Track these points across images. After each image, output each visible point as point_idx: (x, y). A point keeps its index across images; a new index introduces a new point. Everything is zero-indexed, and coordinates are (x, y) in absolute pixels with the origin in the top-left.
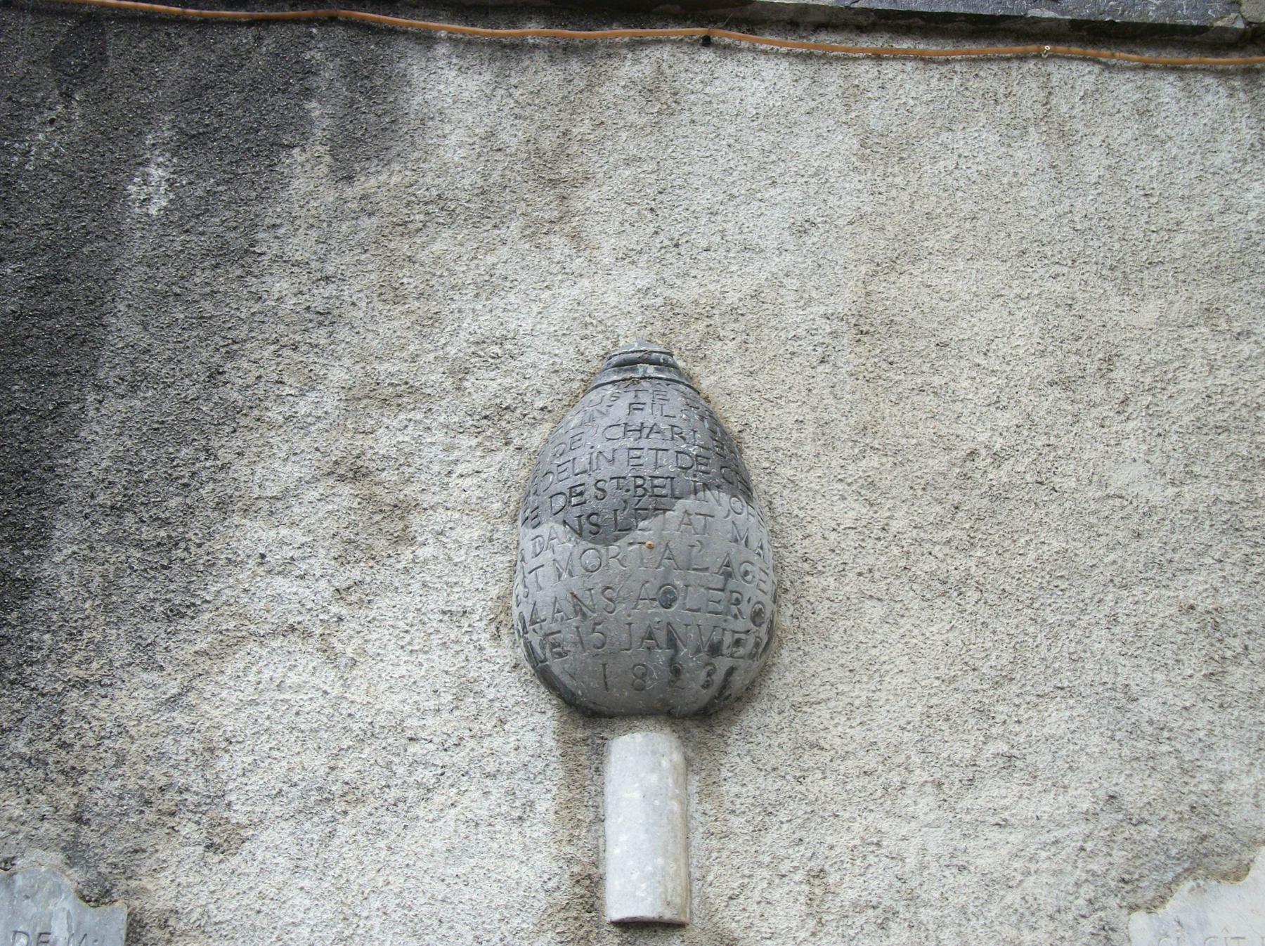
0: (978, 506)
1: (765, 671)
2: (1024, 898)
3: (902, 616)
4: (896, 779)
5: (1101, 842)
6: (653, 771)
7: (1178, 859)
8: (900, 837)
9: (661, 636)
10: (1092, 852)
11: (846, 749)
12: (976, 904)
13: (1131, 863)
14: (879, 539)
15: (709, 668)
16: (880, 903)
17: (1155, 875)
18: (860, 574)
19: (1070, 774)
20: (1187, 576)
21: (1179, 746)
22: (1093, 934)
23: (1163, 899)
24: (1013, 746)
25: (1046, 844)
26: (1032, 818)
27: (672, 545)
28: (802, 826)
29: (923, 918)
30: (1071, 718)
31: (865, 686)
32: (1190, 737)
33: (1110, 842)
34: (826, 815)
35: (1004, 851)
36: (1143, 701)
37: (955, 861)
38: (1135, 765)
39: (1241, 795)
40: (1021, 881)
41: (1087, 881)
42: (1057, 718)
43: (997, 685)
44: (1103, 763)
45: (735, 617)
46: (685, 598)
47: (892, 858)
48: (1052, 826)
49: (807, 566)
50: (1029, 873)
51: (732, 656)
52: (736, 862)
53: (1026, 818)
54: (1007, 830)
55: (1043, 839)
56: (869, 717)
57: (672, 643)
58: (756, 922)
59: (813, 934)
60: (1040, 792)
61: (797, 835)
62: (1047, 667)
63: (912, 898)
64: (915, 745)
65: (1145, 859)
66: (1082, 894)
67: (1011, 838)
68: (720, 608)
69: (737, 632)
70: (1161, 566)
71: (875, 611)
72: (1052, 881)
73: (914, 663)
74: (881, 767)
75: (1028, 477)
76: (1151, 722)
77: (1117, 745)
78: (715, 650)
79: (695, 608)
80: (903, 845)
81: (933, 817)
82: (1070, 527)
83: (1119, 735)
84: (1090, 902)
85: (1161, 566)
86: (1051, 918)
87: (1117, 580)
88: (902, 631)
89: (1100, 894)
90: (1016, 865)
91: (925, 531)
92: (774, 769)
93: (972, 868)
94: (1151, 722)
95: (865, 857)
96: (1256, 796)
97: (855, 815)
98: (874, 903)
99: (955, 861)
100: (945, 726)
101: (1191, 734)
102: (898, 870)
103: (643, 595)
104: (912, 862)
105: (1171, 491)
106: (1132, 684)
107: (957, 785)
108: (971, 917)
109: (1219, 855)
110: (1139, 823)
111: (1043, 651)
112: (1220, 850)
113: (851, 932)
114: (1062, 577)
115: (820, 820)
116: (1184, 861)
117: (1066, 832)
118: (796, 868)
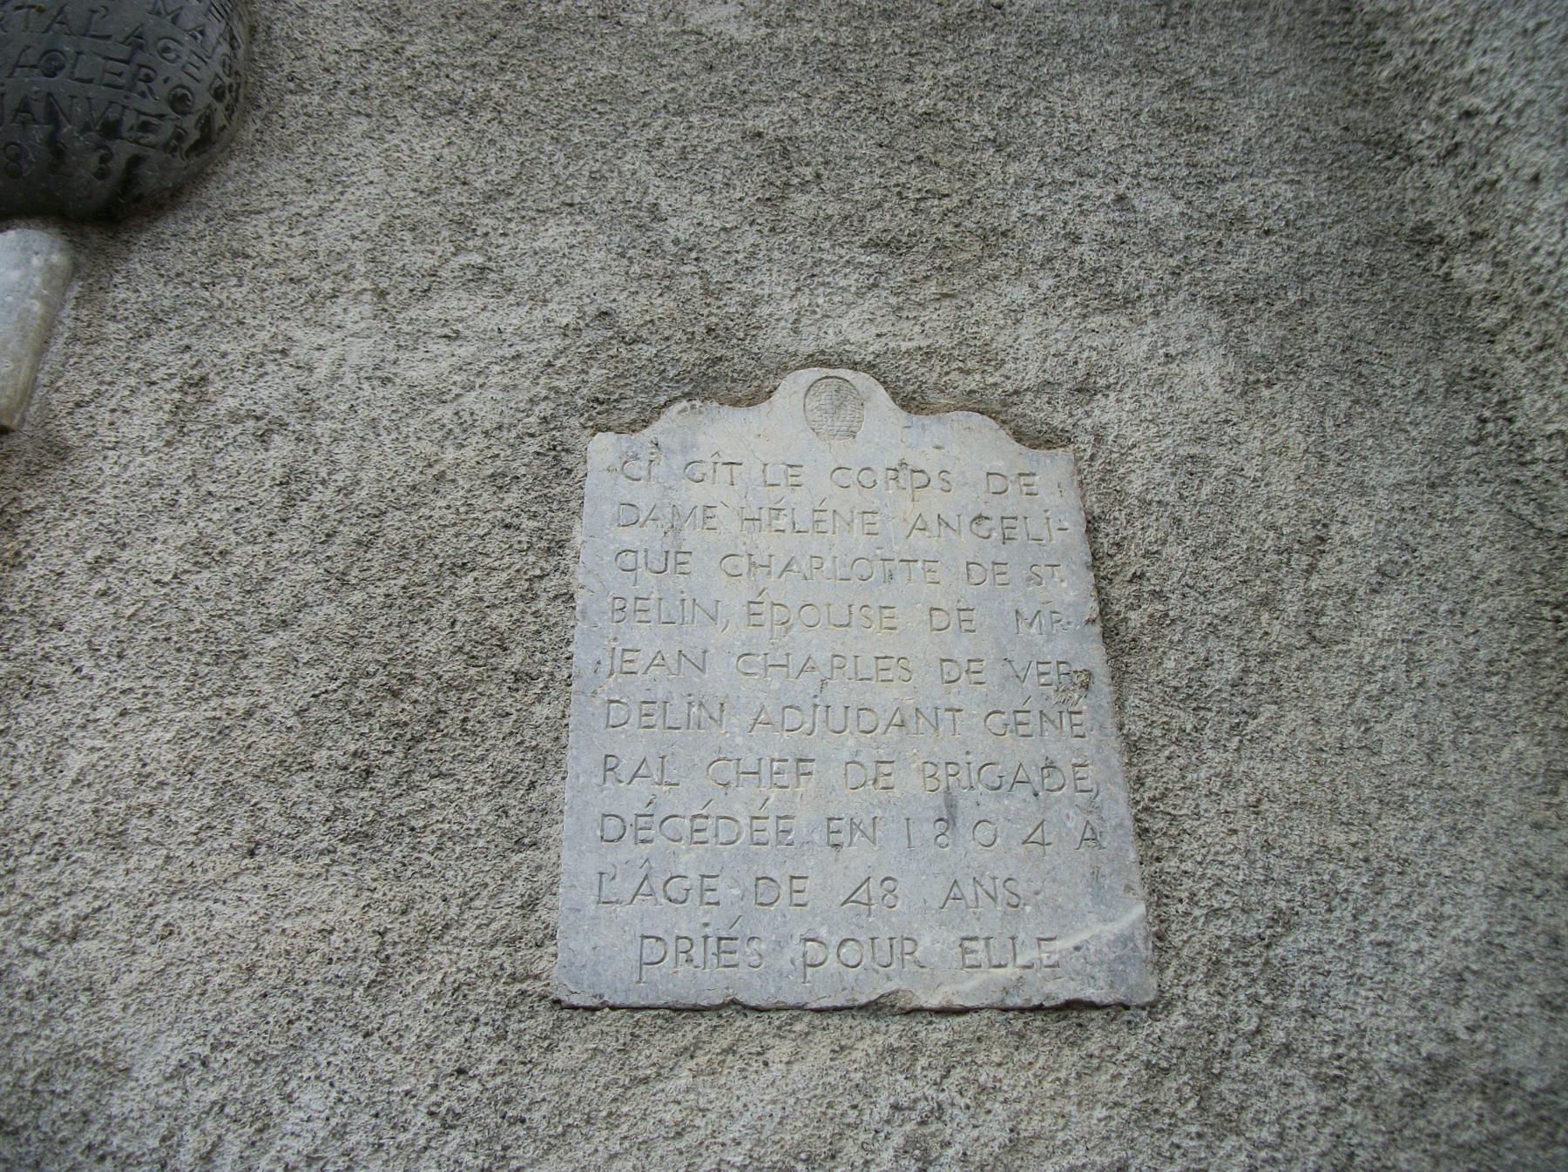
0: (520, 34)
1: (199, 178)
2: (457, 414)
3: (392, 132)
4: (327, 287)
5: (577, 360)
6: (17, 267)
7: (678, 382)
8: (315, 345)
9: (39, 109)
10: (562, 368)
11: (276, 256)
12: (393, 417)
13: (612, 382)
14: (387, 61)
15: (102, 152)
16: (267, 414)
17: (642, 398)
18: (353, 92)
19: (556, 287)
20: (762, 107)
21: (707, 268)
22: (538, 453)
23: (646, 423)
24: (490, 259)
25: (503, 358)
26: (492, 330)
27: (67, 9)
28: (195, 333)
29: (318, 431)
30: (574, 233)
31: (322, 197)
32: (724, 259)
33: (591, 357)
34: (228, 323)
35: (444, 365)
36: (673, 221)
37: (378, 373)
38: (644, 282)
39: (778, 320)
40: (458, 396)
41: (546, 398)
42: (554, 234)
43: (489, 198)
44: (603, 278)
45: (143, 95)
46: (74, 66)
47: (298, 368)
48: (516, 339)
49: (291, 85)
50: (473, 388)
51: (136, 142)
52: (99, 367)
53: (485, 330)
54: (459, 343)
55: (500, 353)
56: (316, 226)
57: (53, 116)
58: (101, 431)
59: (169, 444)
60: (511, 305)
61: (186, 341)
62: (557, 183)
63: (310, 409)
64: (365, 254)
65: (632, 379)
66: (537, 413)
67: (461, 352)
68: (122, 81)
69: (145, 114)
70: (732, 98)
71: (359, 126)
72: (499, 396)
73: (390, 175)
74: (314, 275)
75: (590, 12)
76: (676, 242)
77: (625, 262)
78: (111, 130)
79: (85, 77)
80: (317, 354)
81: (363, 325)
82: (627, 56)
83: (631, 253)
84: (545, 420)
85: (732, 98)
86: (486, 434)
87: (671, 107)
88: (386, 146)
89: (561, 412)
90: (456, 378)
91: (448, 56)
92: (178, 275)
93: (398, 381)
94: (676, 242)
95: (262, 365)
96: (796, 321)
97: (266, 323)
98: (258, 413)
99: (378, 373)
100: (408, 236)
101: (727, 257)
102: (302, 379)
103: (23, 61)
104: (322, 372)
105: (763, 31)
106: (663, 203)
107: (406, 294)
108: (382, 431)
109: (734, 381)
110: (634, 341)
111: (557, 169)
112: (736, 375)
113: (220, 444)
114: (603, 101)
115: (218, 328)
116: (684, 385)
117: (533, 346)
118: (172, 376)
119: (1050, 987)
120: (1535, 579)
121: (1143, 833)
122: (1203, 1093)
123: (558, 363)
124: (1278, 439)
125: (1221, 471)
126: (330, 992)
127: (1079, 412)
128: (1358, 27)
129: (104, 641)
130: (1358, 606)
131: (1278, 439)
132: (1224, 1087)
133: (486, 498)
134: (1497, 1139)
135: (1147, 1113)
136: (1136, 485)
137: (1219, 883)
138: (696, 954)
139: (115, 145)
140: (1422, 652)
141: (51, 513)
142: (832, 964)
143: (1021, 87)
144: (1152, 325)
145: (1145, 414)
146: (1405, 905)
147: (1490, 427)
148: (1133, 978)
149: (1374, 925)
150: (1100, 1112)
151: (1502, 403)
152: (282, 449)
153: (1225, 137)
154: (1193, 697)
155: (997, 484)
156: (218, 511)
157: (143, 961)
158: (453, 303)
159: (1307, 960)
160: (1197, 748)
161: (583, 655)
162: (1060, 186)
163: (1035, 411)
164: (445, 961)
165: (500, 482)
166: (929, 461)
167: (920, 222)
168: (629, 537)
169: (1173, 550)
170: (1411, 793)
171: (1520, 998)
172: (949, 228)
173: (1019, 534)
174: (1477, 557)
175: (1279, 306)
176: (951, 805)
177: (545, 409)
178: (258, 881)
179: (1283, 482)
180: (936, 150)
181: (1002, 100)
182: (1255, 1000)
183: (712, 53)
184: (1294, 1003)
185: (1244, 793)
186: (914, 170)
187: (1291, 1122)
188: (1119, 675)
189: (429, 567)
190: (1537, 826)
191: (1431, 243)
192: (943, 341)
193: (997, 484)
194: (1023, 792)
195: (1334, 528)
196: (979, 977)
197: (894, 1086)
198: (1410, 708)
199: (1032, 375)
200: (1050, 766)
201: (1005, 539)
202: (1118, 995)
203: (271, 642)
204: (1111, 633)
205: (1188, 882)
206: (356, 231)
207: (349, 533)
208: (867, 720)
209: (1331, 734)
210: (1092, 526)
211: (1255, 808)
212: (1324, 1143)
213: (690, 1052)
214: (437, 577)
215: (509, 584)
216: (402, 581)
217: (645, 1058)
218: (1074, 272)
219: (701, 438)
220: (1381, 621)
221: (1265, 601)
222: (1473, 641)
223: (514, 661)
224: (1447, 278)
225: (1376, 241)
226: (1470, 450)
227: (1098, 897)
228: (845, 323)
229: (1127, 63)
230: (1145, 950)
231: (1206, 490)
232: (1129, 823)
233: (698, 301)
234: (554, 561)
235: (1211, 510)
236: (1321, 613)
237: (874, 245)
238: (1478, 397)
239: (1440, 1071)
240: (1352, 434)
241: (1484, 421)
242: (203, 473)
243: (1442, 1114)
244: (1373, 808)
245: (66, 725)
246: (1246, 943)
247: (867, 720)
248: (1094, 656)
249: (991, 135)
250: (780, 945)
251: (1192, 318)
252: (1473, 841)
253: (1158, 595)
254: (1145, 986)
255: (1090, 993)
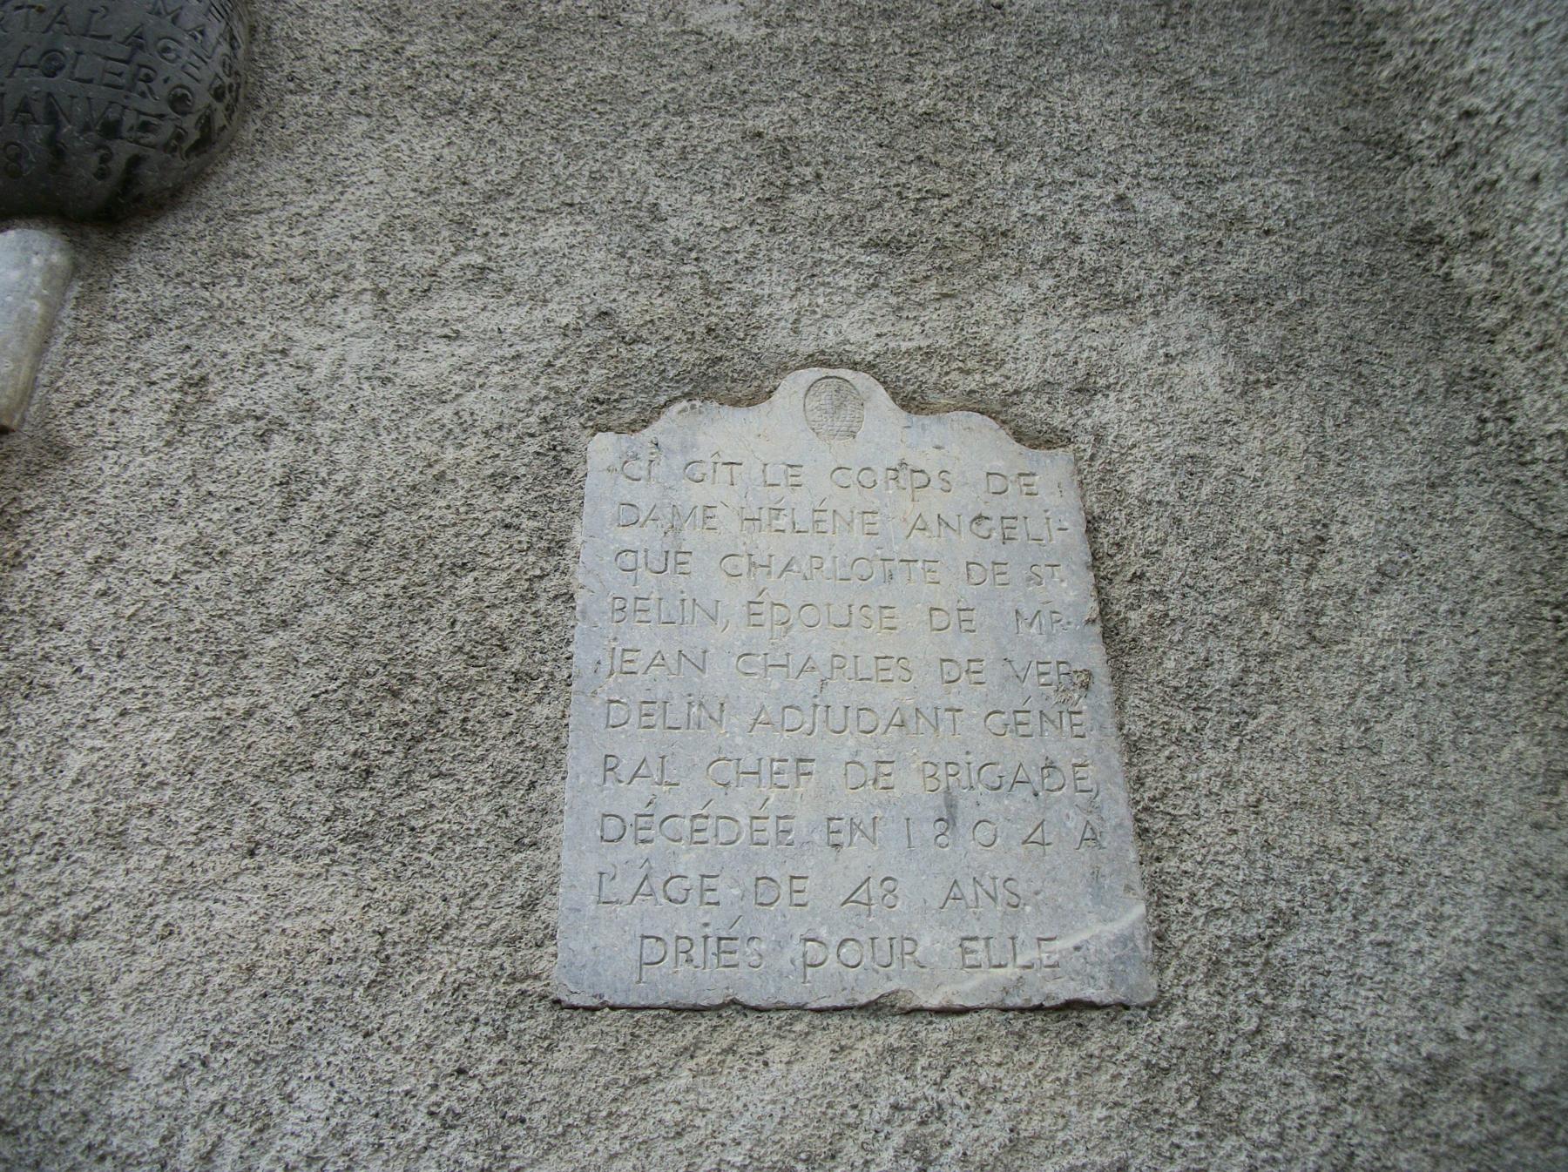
0: (520, 34)
1: (199, 178)
2: (457, 414)
3: (392, 132)
4: (327, 287)
5: (577, 360)
6: (17, 267)
7: (678, 382)
8: (315, 345)
9: (39, 109)
10: (562, 368)
11: (276, 256)
12: (393, 417)
13: (612, 382)
14: (387, 61)
15: (102, 152)
16: (267, 414)
17: (642, 398)
18: (353, 92)
19: (556, 287)
20: (762, 107)
21: (707, 268)
22: (538, 453)
23: (646, 423)
24: (490, 259)
25: (503, 358)
26: (492, 330)
27: (67, 9)
28: (195, 333)
29: (318, 431)
30: (574, 233)
31: (322, 197)
32: (724, 259)
33: (591, 357)
34: (228, 323)
35: (444, 365)
36: (673, 221)
37: (378, 373)
38: (644, 282)
39: (778, 320)
40: (458, 396)
41: (546, 398)
42: (554, 234)
43: (489, 198)
44: (603, 278)
45: (143, 95)
46: (74, 66)
47: (298, 368)
48: (516, 339)
49: (291, 85)
50: (473, 388)
51: (136, 142)
52: (99, 367)
53: (485, 330)
54: (459, 343)
55: (500, 353)
56: (316, 226)
57: (53, 116)
58: (101, 431)
59: (169, 444)
60: (511, 305)
61: (186, 341)
62: (557, 183)
63: (310, 409)
64: (365, 254)
65: (632, 379)
66: (537, 413)
67: (461, 352)
68: (122, 81)
69: (145, 114)
70: (732, 98)
71: (359, 126)
72: (499, 396)
73: (390, 175)
74: (314, 275)
75: (590, 12)
76: (676, 242)
77: (625, 262)
78: (111, 130)
79: (85, 77)
80: (317, 354)
81: (363, 325)
82: (627, 56)
83: (631, 253)
84: (545, 420)
85: (732, 98)
86: (486, 434)
87: (671, 107)
88: (386, 146)
89: (561, 412)
90: (456, 378)
91: (448, 56)
92: (178, 275)
93: (398, 381)
94: (676, 242)
95: (262, 365)
96: (796, 321)
97: (266, 323)
98: (258, 413)
99: (378, 373)
100: (408, 236)
101: (727, 257)
102: (302, 379)
103: (23, 61)
104: (322, 372)
105: (763, 31)
106: (663, 203)
107: (406, 294)
108: (382, 431)
109: (734, 381)
110: (634, 341)
111: (557, 169)
112: (736, 375)
113: (220, 444)
114: (603, 101)
115: (218, 328)
116: (684, 385)
117: (533, 346)
118: (172, 376)
119: (1050, 987)
120: (1535, 579)
121: (1143, 833)
122: (1203, 1093)
123: (558, 363)
124: (1278, 439)
125: (1221, 471)
126: (330, 992)
127: (1079, 412)
128: (1358, 27)
129: (104, 641)
130: (1358, 606)
131: (1278, 439)
132: (1224, 1087)
133: (486, 498)
134: (1497, 1139)
135: (1147, 1113)
136: (1136, 485)
137: (1219, 883)
138: (696, 954)
139: (115, 145)
140: (1422, 652)
141: (51, 513)
142: (832, 964)
143: (1021, 87)
144: (1152, 325)
145: (1145, 414)
146: (1405, 905)
147: (1490, 427)
148: (1133, 978)
149: (1374, 925)
150: (1100, 1112)
151: (1502, 403)
152: (282, 449)
153: (1225, 137)
154: (1193, 697)
155: (997, 484)
156: (218, 511)
157: (143, 961)
158: (453, 303)
159: (1307, 960)
160: (1197, 748)
161: (583, 655)
162: (1060, 186)
163: (1035, 411)
164: (445, 961)
165: (500, 482)
166: (929, 461)
167: (920, 222)
168: (629, 537)
169: (1173, 550)
170: (1411, 793)
171: (1520, 998)
172: (949, 228)
173: (1019, 534)
174: (1477, 557)
175: (1279, 306)
176: (951, 805)
177: (545, 409)
178: (258, 881)
179: (1283, 482)
180: (936, 150)
181: (1002, 100)
182: (1255, 1000)
183: (712, 53)
184: (1294, 1003)
185: (1244, 793)
186: (914, 170)
187: (1291, 1122)
188: (1119, 675)
189: (429, 567)
190: (1537, 826)
191: (1431, 243)
192: (943, 341)
193: (997, 484)
194: (1023, 792)
195: (1334, 528)
196: (979, 977)
197: (894, 1086)
198: (1410, 708)
199: (1032, 375)
200: (1050, 766)
201: (1005, 539)
202: (1118, 995)
203: (271, 642)
204: (1111, 633)
205: (1188, 882)
206: (356, 231)
207: (349, 533)
208: (867, 720)
209: (1331, 734)
210: (1092, 526)
211: (1255, 808)
212: (1324, 1143)
213: (690, 1052)
214: (437, 577)
215: (509, 584)
216: (402, 581)
217: (645, 1058)
218: (1074, 272)
219: (701, 438)
220: (1381, 621)
221: (1265, 601)
222: (1473, 641)
223: (514, 661)
224: (1447, 278)
225: (1376, 241)
226: (1470, 450)
227: (1098, 897)
228: (845, 323)
229: (1127, 63)
230: (1145, 950)
231: (1206, 490)
232: (1129, 823)
233: (698, 301)
234: (554, 561)
235: (1211, 510)
236: (1321, 613)
237: (874, 245)
238: (1478, 397)
239: (1440, 1071)
240: (1352, 434)
241: (1484, 421)
242: (203, 473)
243: (1442, 1114)
244: (1373, 808)
245: (66, 725)
246: (1246, 943)
247: (867, 720)
248: (1094, 656)
249: (991, 135)
250: (780, 945)
251: (1192, 318)
252: (1473, 841)
253: (1158, 595)
254: (1145, 986)
255: (1090, 993)
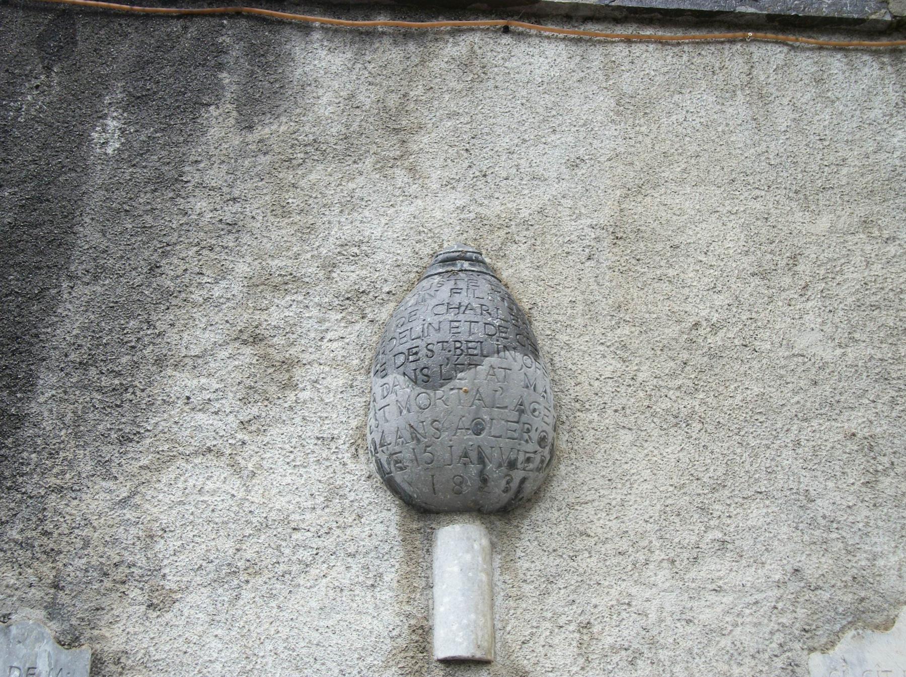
0: (700, 362)
1: (548, 480)
2: (733, 643)
3: (646, 441)
4: (641, 558)
5: (789, 603)
6: (468, 552)
7: (844, 615)
8: (644, 599)
9: (474, 455)
10: (782, 609)
11: (606, 536)
12: (699, 647)
13: (810, 618)
14: (629, 386)
15: (508, 478)
16: (630, 646)
17: (827, 626)
18: (616, 411)
19: (766, 554)
20: (850, 412)
21: (844, 534)
22: (783, 668)
23: (833, 644)
24: (725, 534)
25: (749, 604)
26: (739, 585)
27: (481, 390)
28: (574, 591)
29: (661, 657)
30: (767, 514)
31: (619, 491)
32: (852, 528)
33: (795, 602)
34: (592, 583)
35: (719, 609)
36: (818, 501)
37: (684, 616)
38: (813, 547)
39: (889, 569)
40: (731, 631)
41: (778, 630)
42: (757, 514)
43: (714, 490)
44: (790, 546)
45: (527, 441)
46: (490, 428)
47: (639, 614)
48: (753, 591)
49: (578, 405)
50: (737, 625)
51: (524, 470)
52: (527, 617)
53: (735, 585)
54: (721, 594)
55: (747, 600)
56: (622, 513)
57: (481, 460)
58: (541, 660)
59: (583, 669)
60: (745, 567)
61: (571, 598)
62: (750, 477)
63: (653, 643)
64: (655, 533)
65: (820, 614)
66: (775, 640)
67: (724, 600)
68: (516, 435)
69: (528, 453)
70: (831, 405)
71: (626, 437)
72: (753, 630)
73: (655, 474)
74: (631, 549)
75: (736, 341)
76: (824, 517)
77: (800, 533)
78: (512, 465)
79: (497, 435)
80: (647, 604)
81: (668, 584)
82: (767, 377)
83: (801, 526)
84: (781, 645)
85: (831, 405)
86: (753, 657)
87: (800, 415)
88: (646, 451)
89: (788, 640)
90: (727, 619)
91: (663, 380)
92: (554, 551)
93: (696, 621)
94: (824, 517)
95: (619, 614)
96: (899, 569)
97: (613, 584)
98: (626, 646)
99: (684, 616)
100: (677, 520)
101: (853, 525)
102: (643, 622)
103: (461, 426)
104: (653, 617)
105: (839, 352)
106: (811, 489)
107: (686, 562)
108: (695, 656)
109: (873, 612)
110: (816, 589)
111: (747, 466)
112: (873, 609)
113: (610, 667)
114: (760, 413)
115: (587, 587)
116: (848, 616)
117: (763, 595)
118: (570, 621)
